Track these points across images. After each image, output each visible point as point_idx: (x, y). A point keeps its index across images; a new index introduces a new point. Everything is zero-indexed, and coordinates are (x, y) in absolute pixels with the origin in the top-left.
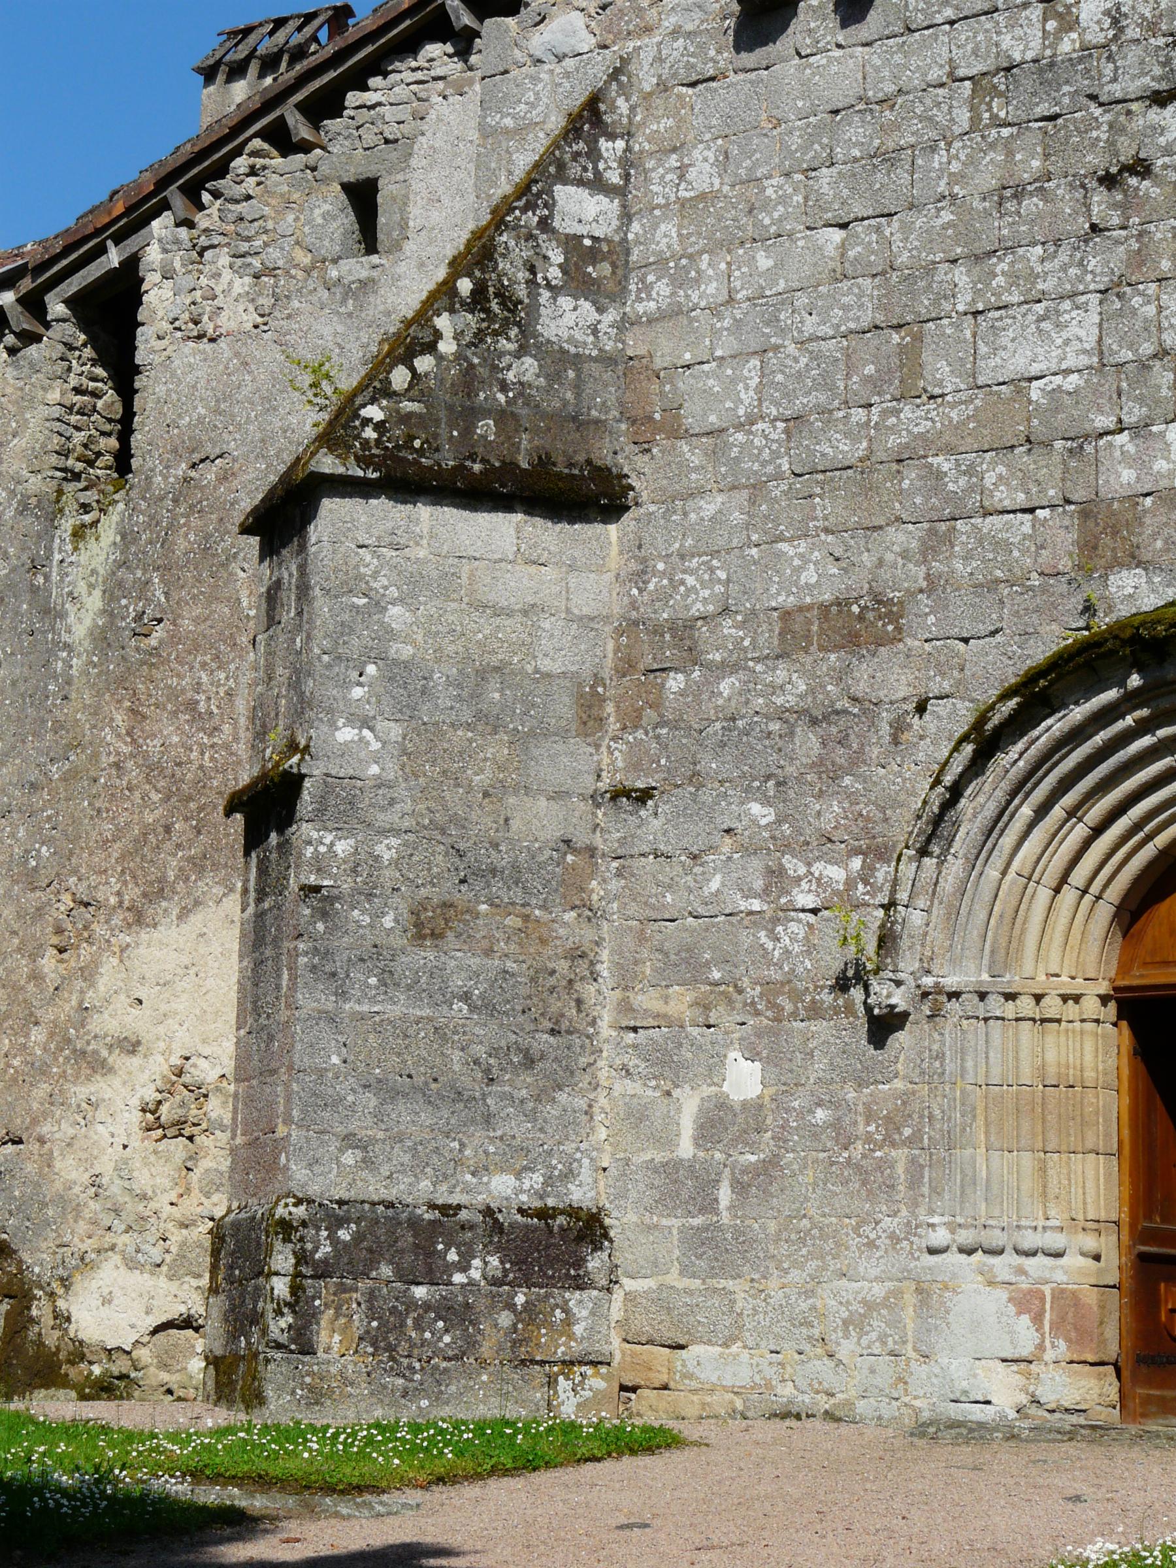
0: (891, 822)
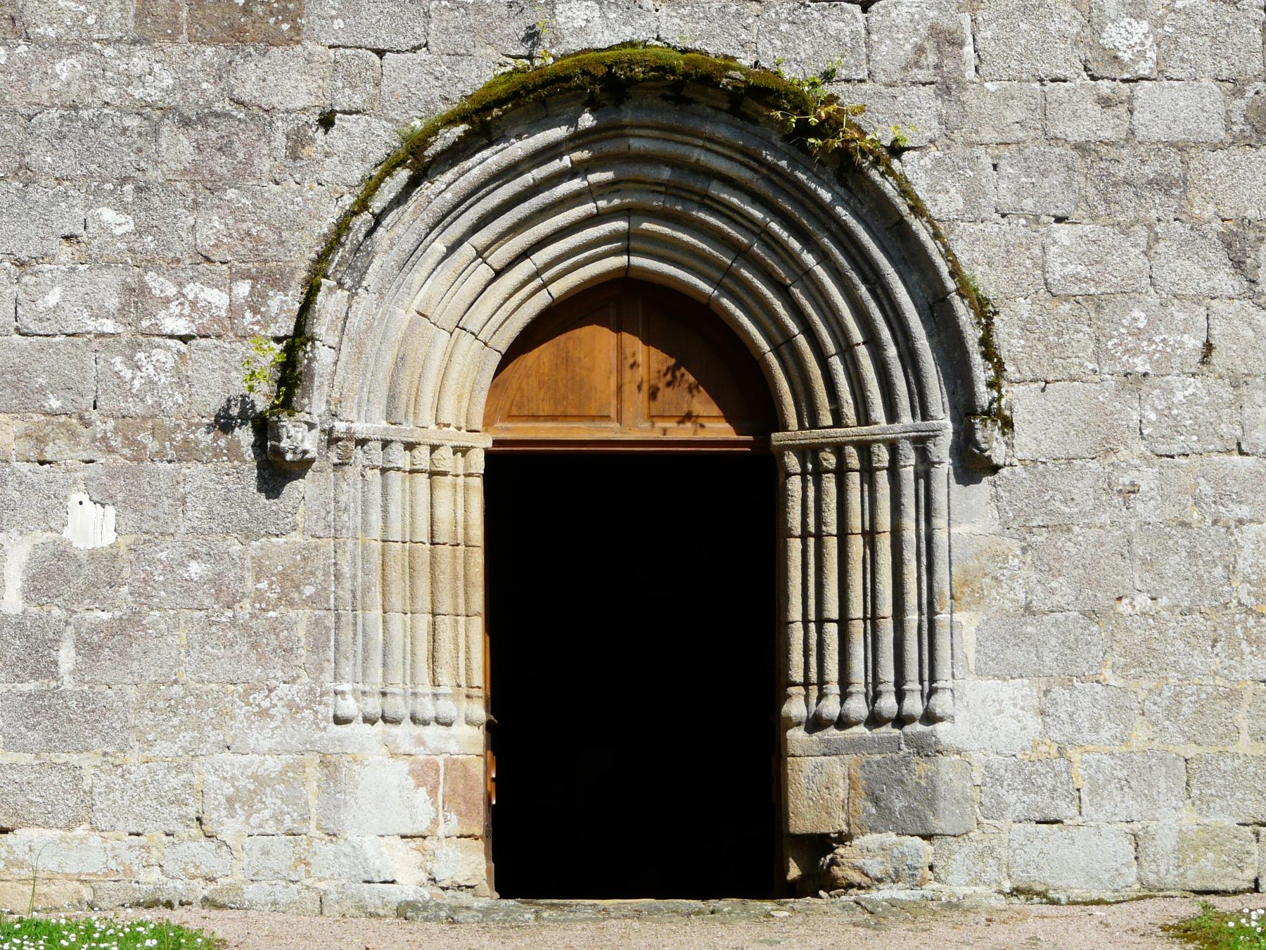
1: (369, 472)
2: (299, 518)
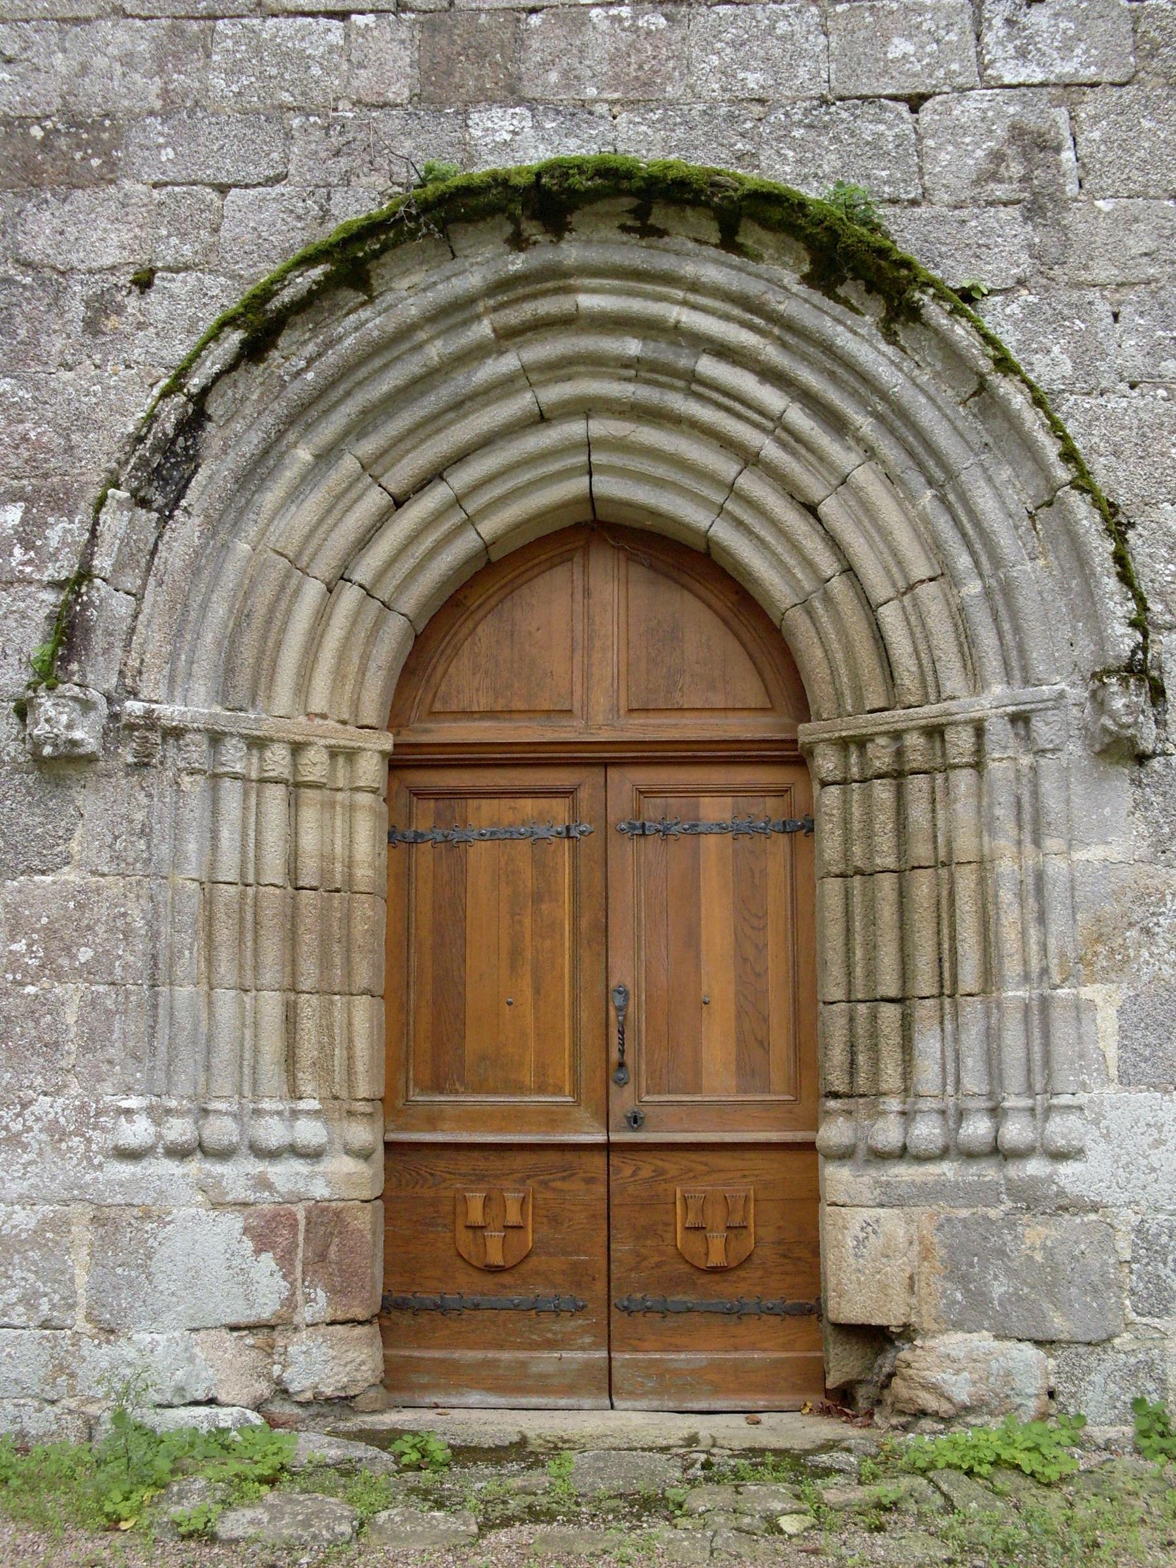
0: (78, 452)
1: (186, 780)
2: (74, 846)
